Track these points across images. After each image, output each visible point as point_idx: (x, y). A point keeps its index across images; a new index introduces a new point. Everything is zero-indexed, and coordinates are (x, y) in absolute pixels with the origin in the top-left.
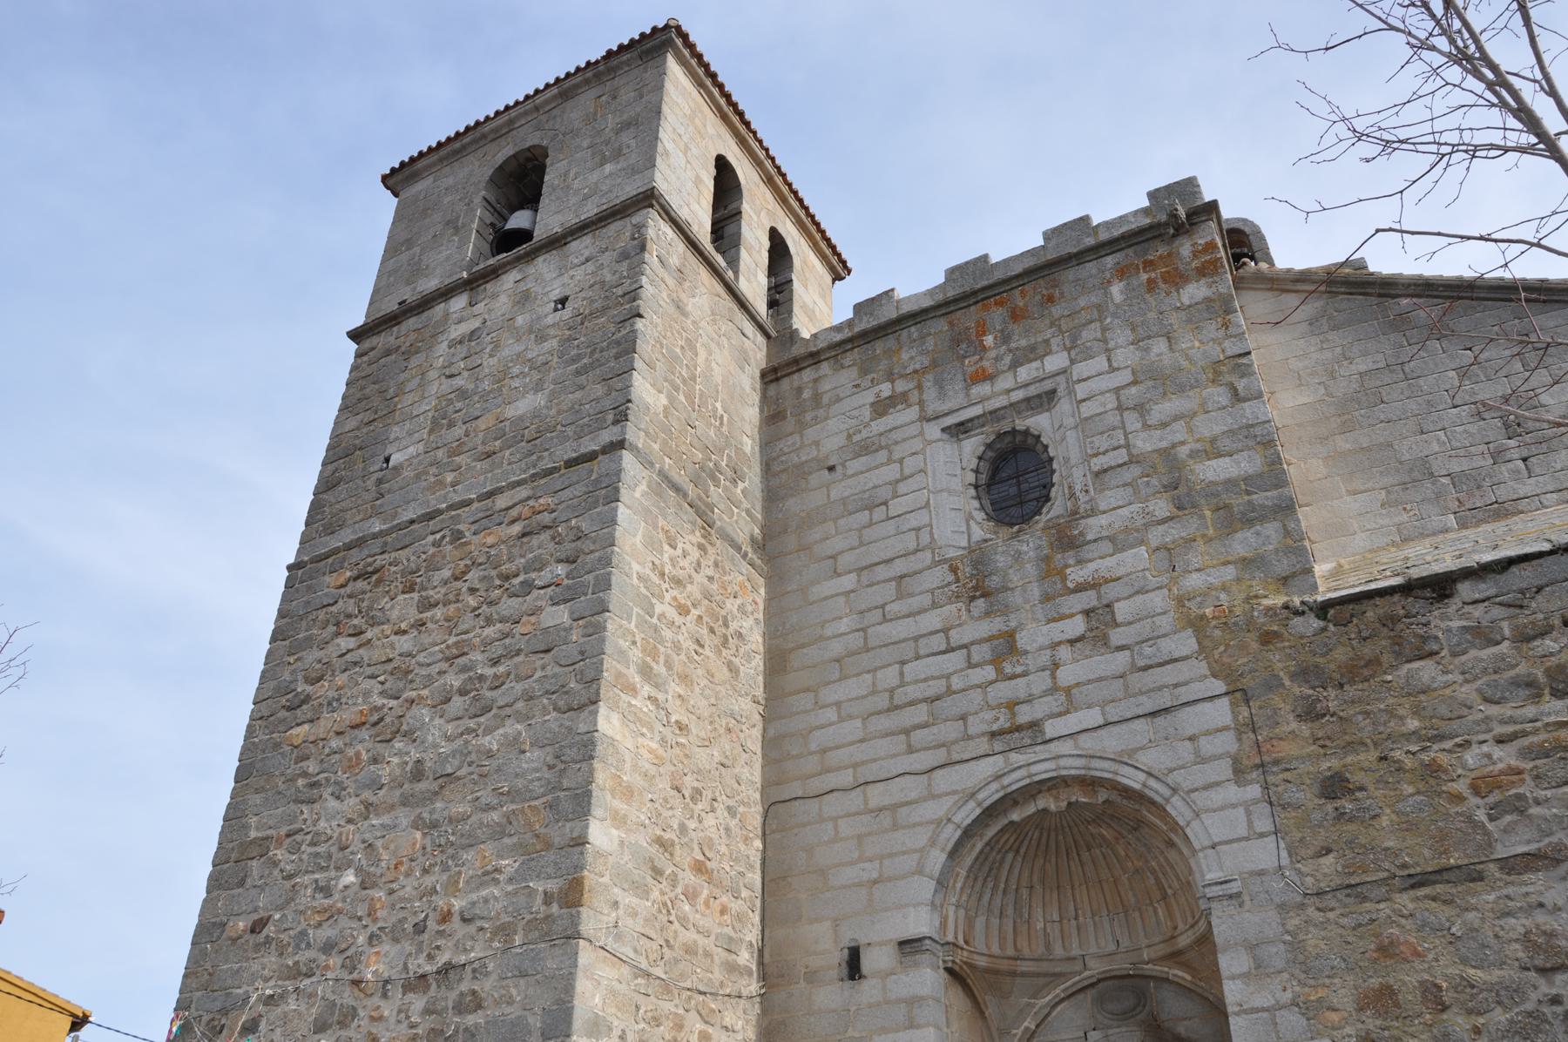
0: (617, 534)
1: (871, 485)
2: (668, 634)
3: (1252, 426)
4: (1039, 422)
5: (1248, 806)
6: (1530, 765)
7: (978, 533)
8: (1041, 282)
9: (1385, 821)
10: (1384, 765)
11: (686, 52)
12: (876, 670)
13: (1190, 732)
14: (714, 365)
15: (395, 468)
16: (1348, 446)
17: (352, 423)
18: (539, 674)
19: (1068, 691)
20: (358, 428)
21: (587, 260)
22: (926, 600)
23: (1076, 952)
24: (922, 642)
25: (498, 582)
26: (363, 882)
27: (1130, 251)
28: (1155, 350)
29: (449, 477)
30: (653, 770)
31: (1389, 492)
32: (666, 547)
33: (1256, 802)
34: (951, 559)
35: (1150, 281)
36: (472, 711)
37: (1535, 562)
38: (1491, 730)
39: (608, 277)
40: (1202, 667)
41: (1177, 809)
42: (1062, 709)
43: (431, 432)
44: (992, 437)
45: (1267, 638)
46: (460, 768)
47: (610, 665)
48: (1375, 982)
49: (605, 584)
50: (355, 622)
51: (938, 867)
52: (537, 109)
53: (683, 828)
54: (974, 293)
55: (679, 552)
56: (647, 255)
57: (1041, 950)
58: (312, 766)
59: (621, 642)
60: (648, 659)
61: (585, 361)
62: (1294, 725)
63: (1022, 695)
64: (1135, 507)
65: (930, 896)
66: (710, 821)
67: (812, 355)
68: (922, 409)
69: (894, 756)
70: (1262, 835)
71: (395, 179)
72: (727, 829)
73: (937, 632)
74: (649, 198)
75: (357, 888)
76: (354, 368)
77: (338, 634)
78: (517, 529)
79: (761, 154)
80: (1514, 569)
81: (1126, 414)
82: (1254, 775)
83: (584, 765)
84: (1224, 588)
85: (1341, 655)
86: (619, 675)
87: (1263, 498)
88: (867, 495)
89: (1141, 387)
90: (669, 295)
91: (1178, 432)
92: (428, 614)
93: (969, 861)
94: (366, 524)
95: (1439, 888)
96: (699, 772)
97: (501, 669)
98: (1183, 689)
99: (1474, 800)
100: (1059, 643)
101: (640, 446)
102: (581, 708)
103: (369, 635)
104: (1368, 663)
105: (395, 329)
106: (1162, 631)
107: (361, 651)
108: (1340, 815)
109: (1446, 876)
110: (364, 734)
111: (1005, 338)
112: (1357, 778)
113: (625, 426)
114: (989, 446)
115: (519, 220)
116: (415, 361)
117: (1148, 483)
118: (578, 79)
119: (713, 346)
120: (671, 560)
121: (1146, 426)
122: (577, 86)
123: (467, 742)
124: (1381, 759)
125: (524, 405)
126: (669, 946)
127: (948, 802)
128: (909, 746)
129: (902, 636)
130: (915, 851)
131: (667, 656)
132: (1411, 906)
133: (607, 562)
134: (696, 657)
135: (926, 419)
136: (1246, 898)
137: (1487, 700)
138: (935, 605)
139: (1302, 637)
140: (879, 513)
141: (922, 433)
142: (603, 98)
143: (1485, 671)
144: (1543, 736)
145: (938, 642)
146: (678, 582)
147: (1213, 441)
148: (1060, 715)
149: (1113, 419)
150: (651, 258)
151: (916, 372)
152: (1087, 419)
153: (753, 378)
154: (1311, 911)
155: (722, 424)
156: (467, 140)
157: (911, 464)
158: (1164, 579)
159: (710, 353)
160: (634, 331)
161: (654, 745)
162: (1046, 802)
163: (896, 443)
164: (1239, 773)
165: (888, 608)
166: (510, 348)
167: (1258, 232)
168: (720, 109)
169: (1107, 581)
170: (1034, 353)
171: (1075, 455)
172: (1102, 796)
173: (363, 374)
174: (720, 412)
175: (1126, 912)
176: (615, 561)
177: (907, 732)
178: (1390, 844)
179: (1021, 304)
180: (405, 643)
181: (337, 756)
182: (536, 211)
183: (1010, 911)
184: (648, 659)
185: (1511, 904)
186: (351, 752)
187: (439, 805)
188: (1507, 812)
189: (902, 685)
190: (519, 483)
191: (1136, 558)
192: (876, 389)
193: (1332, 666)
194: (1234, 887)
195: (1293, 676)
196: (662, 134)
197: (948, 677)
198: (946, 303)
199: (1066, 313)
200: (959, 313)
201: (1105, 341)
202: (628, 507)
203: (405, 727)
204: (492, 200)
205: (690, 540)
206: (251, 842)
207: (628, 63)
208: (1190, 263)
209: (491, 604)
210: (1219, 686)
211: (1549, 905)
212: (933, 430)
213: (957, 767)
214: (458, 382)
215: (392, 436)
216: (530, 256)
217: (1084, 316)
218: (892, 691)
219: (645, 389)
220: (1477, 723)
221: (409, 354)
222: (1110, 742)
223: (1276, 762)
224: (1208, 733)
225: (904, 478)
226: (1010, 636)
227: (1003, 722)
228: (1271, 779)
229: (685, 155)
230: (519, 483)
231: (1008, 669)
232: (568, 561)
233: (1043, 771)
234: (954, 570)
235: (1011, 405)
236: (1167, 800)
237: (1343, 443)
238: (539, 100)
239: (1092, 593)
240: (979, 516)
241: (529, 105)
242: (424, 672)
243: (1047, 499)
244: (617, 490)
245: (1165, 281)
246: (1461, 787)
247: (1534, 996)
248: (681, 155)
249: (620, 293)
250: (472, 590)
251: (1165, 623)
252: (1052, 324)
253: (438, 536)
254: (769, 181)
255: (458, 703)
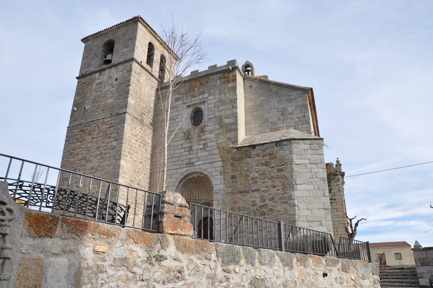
0: (125, 130)
1: (173, 116)
2: (134, 145)
3: (234, 113)
4: (202, 107)
5: (221, 179)
6: (259, 176)
7: (190, 127)
8: (206, 78)
9: (239, 183)
10: (240, 174)
11: (142, 22)
12: (170, 151)
13: (215, 167)
14: (145, 91)
15: (86, 110)
16: (256, 114)
17: (78, 98)
18: (111, 153)
19: (199, 158)
20: (79, 100)
21: (121, 71)
22: (179, 139)
23: (200, 199)
24: (178, 146)
25: (105, 136)
26: (84, 186)
27: (222, 74)
28: (222, 96)
29: (97, 113)
30: (130, 169)
31: (260, 124)
32: (134, 130)
33: (222, 178)
34: (184, 132)
35: (224, 81)
36: (101, 158)
37: (268, 144)
38: (256, 170)
39: (125, 76)
40: (218, 156)
41: (211, 178)
42: (197, 161)
43: (93, 103)
44: (195, 108)
45: (229, 152)
46: (99, 168)
47: (123, 153)
48: (232, 206)
49: (122, 139)
50: (80, 140)
51: (177, 185)
52: (112, 30)
53: (135, 178)
54: (195, 79)
55: (136, 130)
56: (132, 72)
57: (194, 198)
58: (74, 165)
59: (125, 148)
60: (130, 151)
61: (120, 94)
62: (230, 167)
63: (192, 158)
64: (214, 126)
65: (175, 189)
66: (140, 176)
67: (165, 87)
68: (183, 102)
69: (172, 166)
70: (222, 184)
71: (84, 40)
72: (144, 177)
73: (180, 145)
74: (133, 59)
75: (83, 187)
76: (77, 86)
77: (77, 142)
78: (108, 126)
79: (159, 39)
80: (265, 145)
81: (215, 108)
82: (223, 174)
83: (118, 169)
84: (224, 143)
85: (238, 156)
86: (124, 154)
87: (233, 127)
88: (172, 117)
89: (219, 103)
90: (136, 79)
91: (223, 113)
92: (93, 140)
93: (182, 184)
94: (82, 121)
95: (243, 194)
96: (139, 168)
97: (106, 152)
98: (215, 159)
99: (251, 181)
100: (199, 149)
101: (129, 112)
102: (118, 160)
103: (83, 142)
104: (242, 158)
105: (85, 78)
106: (214, 149)
107: (82, 145)
108: (233, 182)
109: (244, 192)
110: (83, 161)
111: (198, 89)
112: (236, 176)
113: (126, 109)
114: (194, 110)
115: (109, 57)
116: (90, 87)
117: (216, 122)
118: (121, 25)
119: (145, 87)
120: (135, 132)
121: (218, 111)
122: (120, 27)
123: (100, 164)
124: (241, 173)
125: (110, 101)
126: (132, 197)
127: (179, 175)
128: (174, 165)
129: (175, 145)
130: (173, 182)
131: (133, 150)
132: (239, 196)
133: (123, 134)
134: (139, 149)
135: (183, 103)
136: (218, 193)
137: (256, 166)
138: (181, 140)
139: (233, 152)
140: (174, 121)
141: (182, 106)
142: (126, 31)
143: (257, 161)
144: (262, 172)
145: (180, 147)
146: (136, 136)
147: (228, 115)
148: (197, 162)
149: (213, 109)
150: (133, 73)
151: (183, 93)
152: (209, 108)
153: (154, 91)
154: (226, 196)
155: (146, 103)
156: (98, 35)
157: (180, 112)
158: (216, 140)
159: (145, 88)
160: (129, 89)
161: (130, 165)
162: (194, 175)
163: (178, 108)
164: (221, 174)
165: (173, 140)
166: (107, 88)
167: (252, 64)
168: (150, 32)
169: (207, 139)
170: (203, 93)
171: (206, 115)
172: (203, 175)
173: (79, 87)
174: (146, 100)
175: (208, 193)
176: (124, 134)
177: (174, 162)
178: (238, 187)
179: (202, 82)
180: (89, 145)
181: (79, 164)
182: (113, 54)
183: (190, 192)
184: (130, 151)
185: (252, 196)
186: (81, 164)
187: (96, 174)
188: (254, 183)
189: (174, 154)
190: (108, 117)
191: (212, 136)
192: (176, 96)
193: (237, 158)
194: (217, 191)
195: (231, 159)
196: (136, 43)
197: (181, 153)
198: (190, 80)
199: (209, 85)
200: (192, 82)
201: (214, 93)
202: (127, 124)
203: (90, 160)
204: (104, 50)
205: (138, 128)
206: (65, 178)
207: (131, 23)
208: (231, 78)
209: (104, 140)
210: (220, 159)
211: (256, 197)
212: (185, 106)
213: (181, 169)
214: (98, 93)
215: (86, 103)
216: (111, 67)
217: (212, 87)
218: (172, 155)
219: (131, 101)
220: (254, 169)
221: (88, 84)
222: (204, 167)
223: (226, 173)
224: (218, 167)
225: (178, 115)
226: (191, 147)
227: (189, 162)
228: (225, 175)
229: (141, 46)
230: (108, 117)
231: (190, 153)
232: (117, 133)
233: (194, 171)
234: (184, 134)
235: (198, 103)
236: (210, 177)
237: (255, 114)
238: (113, 28)
239: (205, 141)
240: (190, 123)
241: (111, 29)
242: (93, 151)
243: (202, 122)
244: (125, 121)
245: (226, 82)
246: (250, 179)
247: (251, 209)
248: (140, 46)
249: (127, 80)
250: (101, 137)
251: (215, 147)
252: (207, 88)
253: (95, 125)
254: (161, 44)
255: (99, 157)
